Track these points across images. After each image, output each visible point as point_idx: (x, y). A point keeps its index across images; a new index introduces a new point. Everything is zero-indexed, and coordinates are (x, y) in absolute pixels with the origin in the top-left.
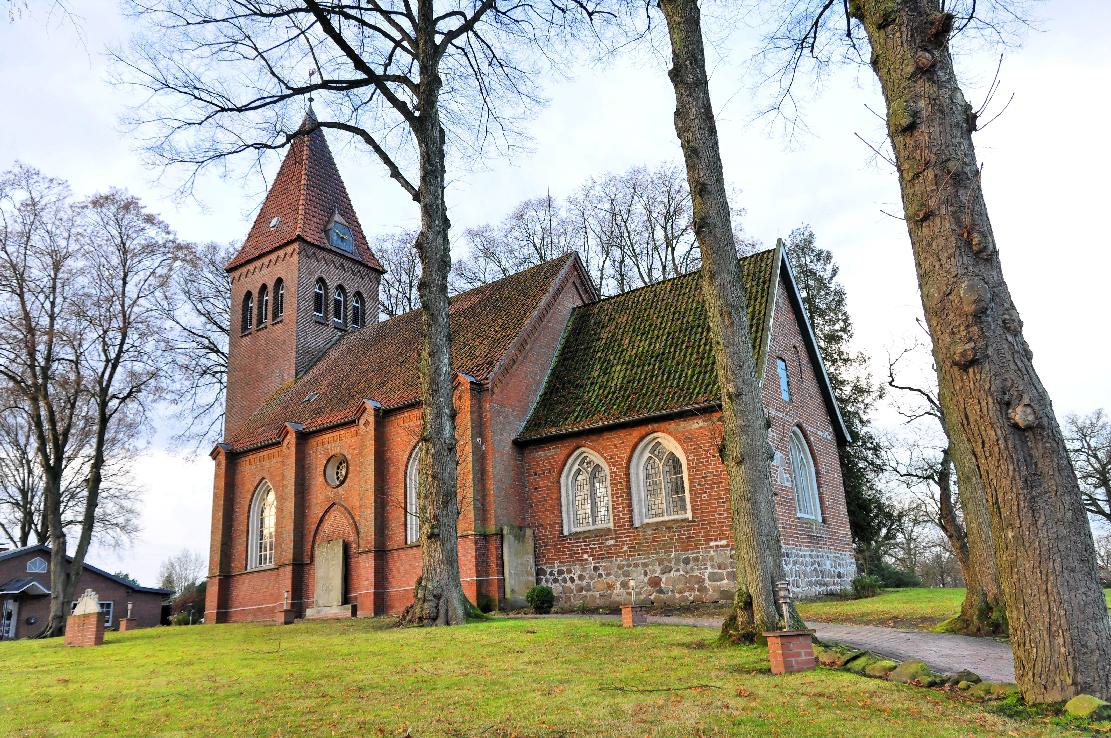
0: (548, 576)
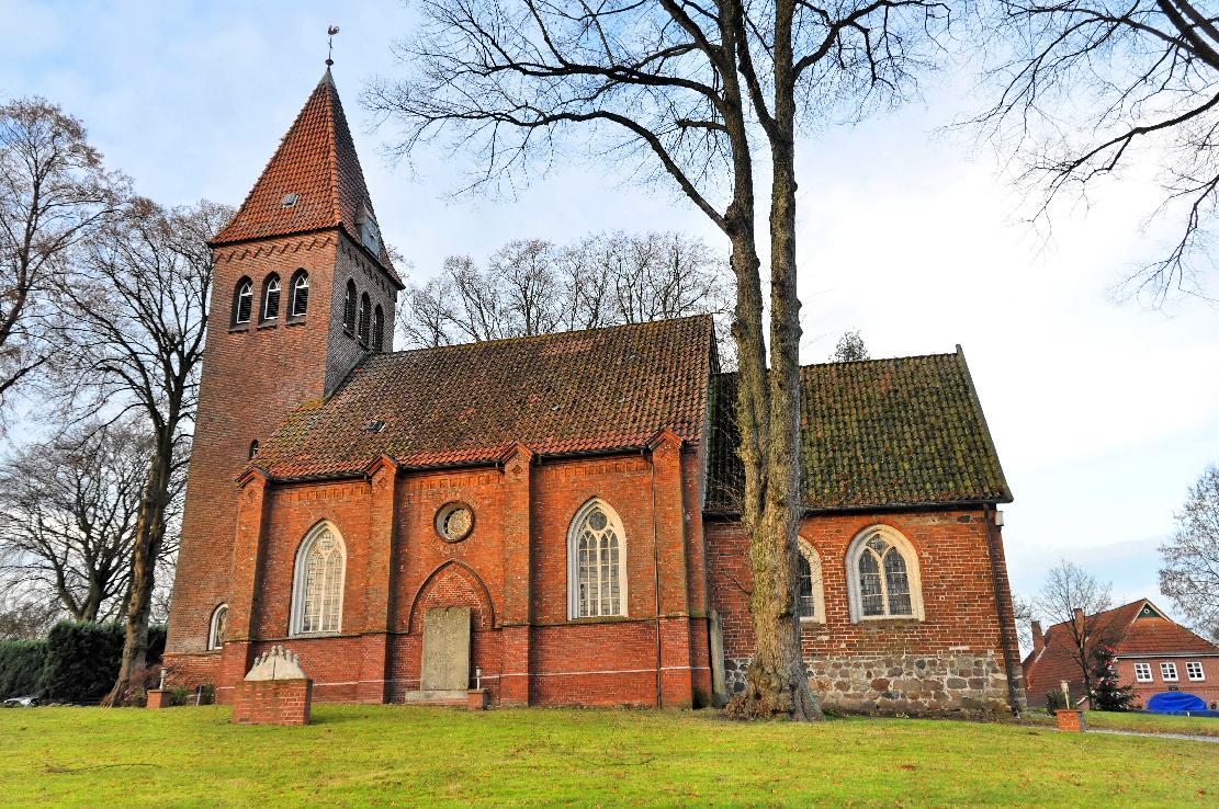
0: (739, 671)
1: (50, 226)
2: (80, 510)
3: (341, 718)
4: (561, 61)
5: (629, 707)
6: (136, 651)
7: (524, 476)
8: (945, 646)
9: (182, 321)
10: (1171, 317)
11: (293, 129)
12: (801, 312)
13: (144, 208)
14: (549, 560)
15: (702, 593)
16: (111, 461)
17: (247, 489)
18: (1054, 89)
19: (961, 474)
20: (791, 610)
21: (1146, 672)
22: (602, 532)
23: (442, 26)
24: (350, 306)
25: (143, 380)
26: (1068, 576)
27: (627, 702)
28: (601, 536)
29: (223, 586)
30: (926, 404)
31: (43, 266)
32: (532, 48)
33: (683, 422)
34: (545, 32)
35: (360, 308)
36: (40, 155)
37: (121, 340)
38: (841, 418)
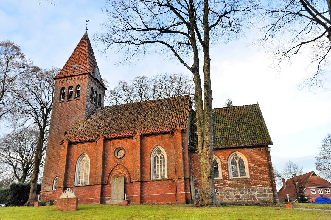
1: (11, 74)
2: (20, 152)
3: (87, 209)
4: (146, 27)
5: (168, 204)
6: (34, 191)
7: (139, 140)
8: (256, 185)
9: (47, 99)
10: (315, 94)
11: (77, 47)
12: (212, 94)
13: (36, 69)
14: (146, 163)
15: (188, 171)
16: (29, 138)
17: (63, 145)
18: (280, 32)
19: (259, 137)
20: (211, 176)
21: (314, 192)
22: (160, 155)
23: (114, 18)
24: (92, 95)
25: (36, 116)
26: (291, 165)
27: (167, 202)
28: (160, 156)
29: (56, 173)
30: (249, 118)
31: (9, 85)
32: (138, 24)
33: (182, 124)
34: (142, 20)
35: (95, 95)
36: (8, 56)
37: (30, 105)
38: (225, 122)
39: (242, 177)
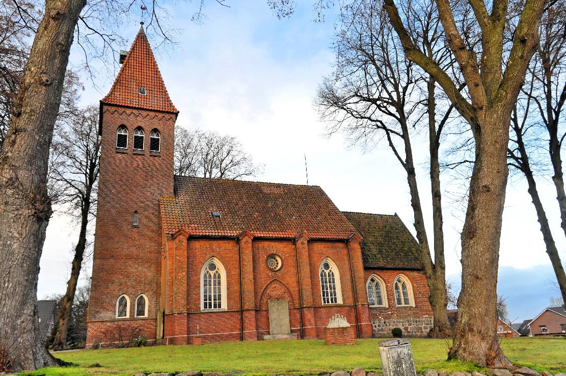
28: (213, 273)
39: (406, 305)
